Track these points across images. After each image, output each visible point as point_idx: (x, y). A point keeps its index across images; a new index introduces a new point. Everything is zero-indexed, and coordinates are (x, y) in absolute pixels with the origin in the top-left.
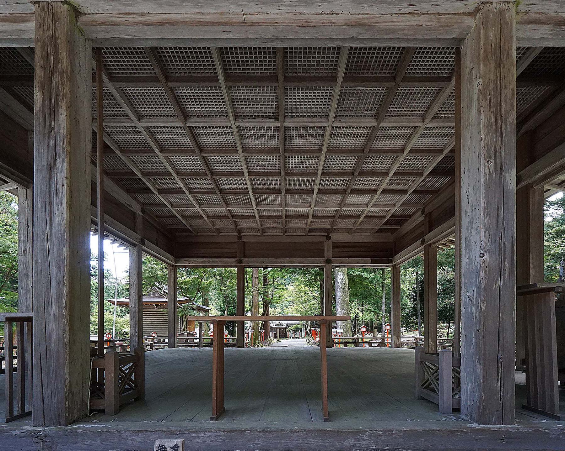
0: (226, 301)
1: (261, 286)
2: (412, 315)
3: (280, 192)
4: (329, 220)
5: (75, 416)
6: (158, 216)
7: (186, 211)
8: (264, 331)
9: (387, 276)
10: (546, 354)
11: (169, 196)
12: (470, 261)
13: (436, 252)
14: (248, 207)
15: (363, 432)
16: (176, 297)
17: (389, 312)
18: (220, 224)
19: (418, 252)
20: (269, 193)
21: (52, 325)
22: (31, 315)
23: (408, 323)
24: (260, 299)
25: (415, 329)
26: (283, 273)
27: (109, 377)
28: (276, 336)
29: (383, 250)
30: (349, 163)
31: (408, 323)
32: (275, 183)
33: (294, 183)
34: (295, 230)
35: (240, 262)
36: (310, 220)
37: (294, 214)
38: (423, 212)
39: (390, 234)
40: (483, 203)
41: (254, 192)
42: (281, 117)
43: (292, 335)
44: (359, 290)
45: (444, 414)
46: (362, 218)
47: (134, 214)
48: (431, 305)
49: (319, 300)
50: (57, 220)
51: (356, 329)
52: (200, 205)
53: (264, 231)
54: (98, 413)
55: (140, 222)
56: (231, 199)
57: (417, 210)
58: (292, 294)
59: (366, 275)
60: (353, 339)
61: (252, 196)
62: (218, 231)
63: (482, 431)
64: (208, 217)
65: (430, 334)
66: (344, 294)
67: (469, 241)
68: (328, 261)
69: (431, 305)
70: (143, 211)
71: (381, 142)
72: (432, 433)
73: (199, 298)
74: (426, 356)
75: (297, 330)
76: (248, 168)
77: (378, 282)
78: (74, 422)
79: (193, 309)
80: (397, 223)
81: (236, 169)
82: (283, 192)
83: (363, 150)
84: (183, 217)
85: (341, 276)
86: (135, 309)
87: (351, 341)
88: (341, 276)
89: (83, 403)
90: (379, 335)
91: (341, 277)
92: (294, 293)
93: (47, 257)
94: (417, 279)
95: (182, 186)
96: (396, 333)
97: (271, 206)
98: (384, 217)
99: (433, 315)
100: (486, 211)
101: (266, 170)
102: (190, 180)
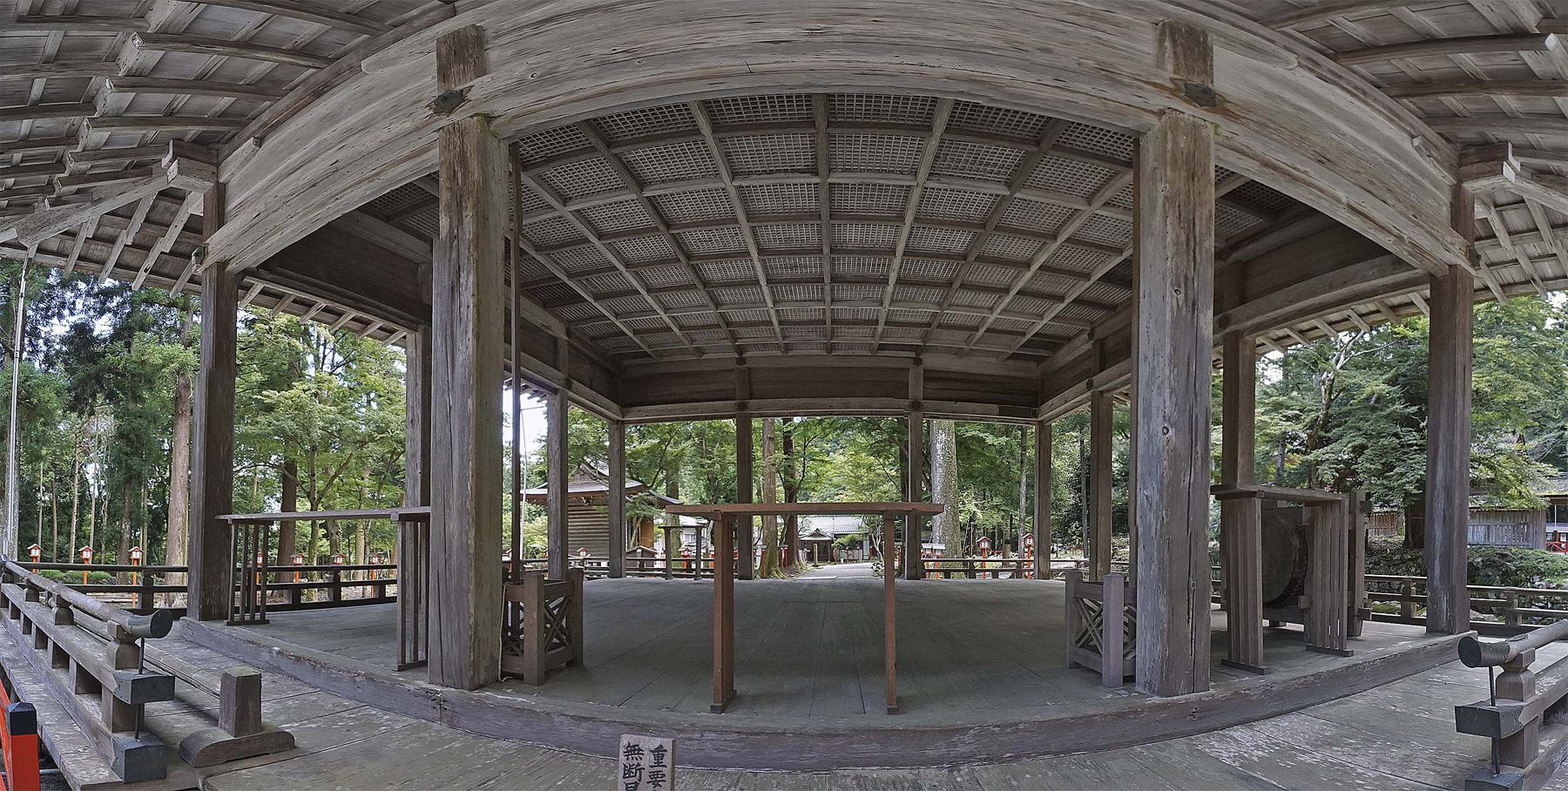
0: (713, 486)
1: (780, 455)
2: (1074, 520)
3: (821, 280)
4: (919, 331)
5: (482, 677)
7: (642, 321)
8: (788, 548)
9: (1030, 443)
10: (1250, 577)
12: (1150, 437)
13: (1111, 405)
14: (761, 305)
16: (622, 483)
17: (1030, 512)
18: (702, 339)
19: (1081, 403)
20: (798, 282)
21: (453, 526)
22: (427, 509)
23: (1066, 534)
24: (779, 482)
25: (1079, 547)
26: (824, 429)
27: (530, 619)
28: (810, 558)
29: (1021, 393)
30: (958, 241)
31: (1066, 539)
32: (810, 265)
33: (848, 266)
34: (851, 346)
36: (880, 328)
37: (848, 316)
38: (1091, 335)
39: (1033, 364)
41: (769, 281)
43: (843, 554)
44: (976, 467)
45: (1111, 687)
46: (982, 331)
49: (898, 482)
50: (460, 358)
51: (970, 545)
52: (666, 310)
53: (788, 348)
54: (514, 678)
56: (726, 295)
57: (1082, 332)
59: (990, 439)
60: (965, 563)
61: (765, 288)
62: (700, 351)
63: (1164, 706)
64: (681, 328)
65: (1098, 554)
66: (948, 473)
67: (1148, 403)
68: (916, 406)
71: (1013, 217)
72: (1088, 721)
73: (660, 484)
74: (1082, 589)
75: (854, 544)
77: (1012, 453)
78: (480, 687)
79: (651, 504)
80: (1046, 346)
82: (827, 280)
83: (982, 226)
84: (635, 332)
85: (942, 437)
86: (555, 504)
87: (960, 566)
88: (942, 437)
89: (494, 660)
90: (1013, 556)
91: (942, 438)
92: (847, 469)
93: (449, 415)
94: (1082, 452)
96: (1043, 552)
97: (803, 305)
98: (1024, 334)
99: (1105, 522)
101: (794, 245)
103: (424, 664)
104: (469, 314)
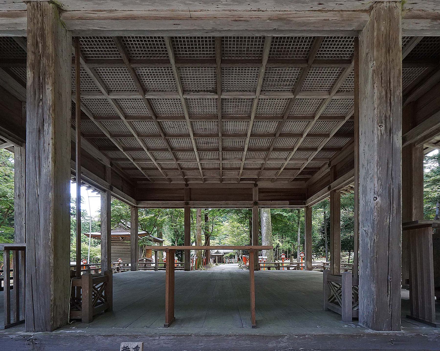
0: (176, 234)
1: (203, 222)
2: (321, 245)
3: (218, 150)
4: (256, 172)
5: (59, 324)
6: (123, 168)
7: (145, 164)
8: (206, 258)
9: (301, 215)
11: (132, 153)
12: (366, 203)
13: (340, 196)
14: (193, 161)
16: (137, 231)
17: (303, 243)
18: (171, 174)
19: (326, 197)
20: (209, 150)
21: (41, 253)
22: (24, 245)
23: (318, 251)
24: (203, 233)
25: (323, 256)
26: (220, 213)
27: (85, 293)
28: (215, 262)
29: (298, 195)
30: (272, 127)
31: (317, 252)
32: (214, 142)
33: (229, 143)
34: (230, 179)
36: (241, 171)
37: (229, 166)
38: (329, 165)
39: (303, 182)
41: (198, 149)
42: (219, 91)
43: (228, 260)
44: (280, 226)
45: (346, 322)
46: (282, 169)
47: (104, 167)
49: (249, 233)
50: (44, 171)
51: (277, 256)
52: (156, 160)
53: (205, 180)
54: (76, 321)
55: (109, 173)
56: (180, 155)
57: (325, 164)
58: (227, 229)
59: (285, 214)
60: (275, 264)
61: (196, 153)
62: (170, 180)
63: (375, 335)
64: (162, 169)
65: (335, 260)
66: (268, 229)
67: (365, 188)
68: (256, 203)
70: (111, 164)
71: (297, 110)
72: (337, 337)
73: (155, 232)
74: (332, 277)
75: (232, 257)
76: (193, 131)
77: (294, 220)
78: (58, 328)
79: (150, 240)
80: (309, 173)
81: (183, 131)
82: (220, 149)
83: (283, 117)
84: (143, 169)
85: (265, 215)
86: (105, 241)
87: (273, 265)
88: (265, 215)
89: (65, 314)
90: (295, 261)
91: (265, 215)
92: (229, 228)
93: (37, 200)
94: (325, 217)
95: (142, 145)
96: (309, 259)
97: (211, 161)
98: (299, 169)
99: (337, 246)
101: (207, 133)
102: (148, 140)
103: (23, 322)
104: (50, 149)
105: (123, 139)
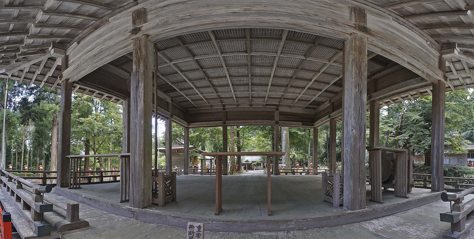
0: (215, 147)
1: (236, 137)
2: (325, 157)
3: (248, 85)
4: (278, 100)
5: (146, 205)
6: (179, 102)
7: (194, 97)
8: (238, 166)
9: (311, 134)
11: (185, 91)
12: (348, 132)
13: (336, 122)
14: (230, 92)
15: (291, 221)
16: (188, 146)
17: (311, 155)
18: (212, 102)
19: (327, 122)
20: (241, 85)
23: (322, 161)
24: (235, 146)
25: (326, 165)
26: (249, 130)
27: (160, 187)
28: (245, 169)
29: (308, 119)
31: (322, 163)
32: (245, 80)
33: (256, 80)
34: (257, 105)
35: (225, 123)
36: (266, 99)
37: (256, 96)
38: (330, 101)
39: (312, 110)
40: (353, 105)
41: (232, 85)
42: (249, 51)
43: (255, 167)
44: (295, 141)
45: (336, 208)
46: (297, 100)
47: (168, 103)
48: (332, 154)
49: (272, 146)
51: (293, 165)
52: (201, 94)
53: (238, 105)
54: (155, 205)
55: (170, 107)
56: (219, 89)
57: (327, 100)
58: (255, 141)
59: (299, 133)
60: (292, 170)
61: (231, 87)
62: (212, 106)
63: (352, 213)
64: (206, 99)
65: (332, 167)
66: (287, 143)
67: (347, 122)
68: (277, 123)
69: (332, 154)
70: (172, 101)
72: (329, 218)
73: (199, 146)
74: (327, 178)
75: (258, 164)
76: (229, 74)
77: (306, 137)
78: (145, 208)
79: (197, 152)
80: (316, 105)
81: (222, 74)
82: (250, 84)
83: (297, 68)
84: (192, 100)
85: (285, 132)
86: (168, 152)
87: (290, 171)
88: (285, 132)
89: (149, 200)
90: (306, 168)
91: (285, 132)
92: (256, 142)
94: (327, 137)
95: (192, 86)
96: (315, 167)
97: (243, 92)
98: (310, 101)
99: (334, 158)
100: (355, 109)
101: (240, 74)
102: (196, 82)
105: (179, 84)
